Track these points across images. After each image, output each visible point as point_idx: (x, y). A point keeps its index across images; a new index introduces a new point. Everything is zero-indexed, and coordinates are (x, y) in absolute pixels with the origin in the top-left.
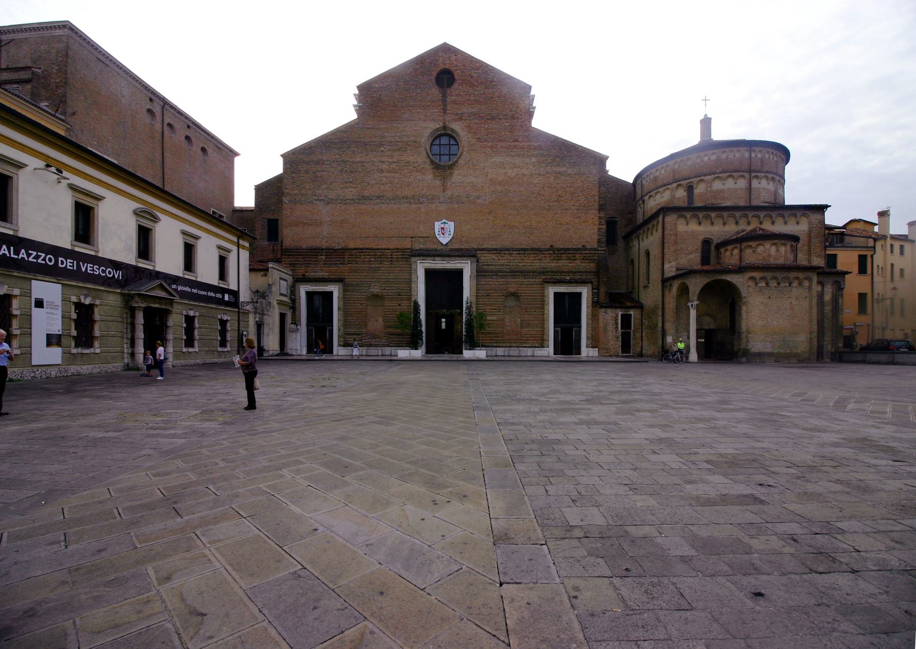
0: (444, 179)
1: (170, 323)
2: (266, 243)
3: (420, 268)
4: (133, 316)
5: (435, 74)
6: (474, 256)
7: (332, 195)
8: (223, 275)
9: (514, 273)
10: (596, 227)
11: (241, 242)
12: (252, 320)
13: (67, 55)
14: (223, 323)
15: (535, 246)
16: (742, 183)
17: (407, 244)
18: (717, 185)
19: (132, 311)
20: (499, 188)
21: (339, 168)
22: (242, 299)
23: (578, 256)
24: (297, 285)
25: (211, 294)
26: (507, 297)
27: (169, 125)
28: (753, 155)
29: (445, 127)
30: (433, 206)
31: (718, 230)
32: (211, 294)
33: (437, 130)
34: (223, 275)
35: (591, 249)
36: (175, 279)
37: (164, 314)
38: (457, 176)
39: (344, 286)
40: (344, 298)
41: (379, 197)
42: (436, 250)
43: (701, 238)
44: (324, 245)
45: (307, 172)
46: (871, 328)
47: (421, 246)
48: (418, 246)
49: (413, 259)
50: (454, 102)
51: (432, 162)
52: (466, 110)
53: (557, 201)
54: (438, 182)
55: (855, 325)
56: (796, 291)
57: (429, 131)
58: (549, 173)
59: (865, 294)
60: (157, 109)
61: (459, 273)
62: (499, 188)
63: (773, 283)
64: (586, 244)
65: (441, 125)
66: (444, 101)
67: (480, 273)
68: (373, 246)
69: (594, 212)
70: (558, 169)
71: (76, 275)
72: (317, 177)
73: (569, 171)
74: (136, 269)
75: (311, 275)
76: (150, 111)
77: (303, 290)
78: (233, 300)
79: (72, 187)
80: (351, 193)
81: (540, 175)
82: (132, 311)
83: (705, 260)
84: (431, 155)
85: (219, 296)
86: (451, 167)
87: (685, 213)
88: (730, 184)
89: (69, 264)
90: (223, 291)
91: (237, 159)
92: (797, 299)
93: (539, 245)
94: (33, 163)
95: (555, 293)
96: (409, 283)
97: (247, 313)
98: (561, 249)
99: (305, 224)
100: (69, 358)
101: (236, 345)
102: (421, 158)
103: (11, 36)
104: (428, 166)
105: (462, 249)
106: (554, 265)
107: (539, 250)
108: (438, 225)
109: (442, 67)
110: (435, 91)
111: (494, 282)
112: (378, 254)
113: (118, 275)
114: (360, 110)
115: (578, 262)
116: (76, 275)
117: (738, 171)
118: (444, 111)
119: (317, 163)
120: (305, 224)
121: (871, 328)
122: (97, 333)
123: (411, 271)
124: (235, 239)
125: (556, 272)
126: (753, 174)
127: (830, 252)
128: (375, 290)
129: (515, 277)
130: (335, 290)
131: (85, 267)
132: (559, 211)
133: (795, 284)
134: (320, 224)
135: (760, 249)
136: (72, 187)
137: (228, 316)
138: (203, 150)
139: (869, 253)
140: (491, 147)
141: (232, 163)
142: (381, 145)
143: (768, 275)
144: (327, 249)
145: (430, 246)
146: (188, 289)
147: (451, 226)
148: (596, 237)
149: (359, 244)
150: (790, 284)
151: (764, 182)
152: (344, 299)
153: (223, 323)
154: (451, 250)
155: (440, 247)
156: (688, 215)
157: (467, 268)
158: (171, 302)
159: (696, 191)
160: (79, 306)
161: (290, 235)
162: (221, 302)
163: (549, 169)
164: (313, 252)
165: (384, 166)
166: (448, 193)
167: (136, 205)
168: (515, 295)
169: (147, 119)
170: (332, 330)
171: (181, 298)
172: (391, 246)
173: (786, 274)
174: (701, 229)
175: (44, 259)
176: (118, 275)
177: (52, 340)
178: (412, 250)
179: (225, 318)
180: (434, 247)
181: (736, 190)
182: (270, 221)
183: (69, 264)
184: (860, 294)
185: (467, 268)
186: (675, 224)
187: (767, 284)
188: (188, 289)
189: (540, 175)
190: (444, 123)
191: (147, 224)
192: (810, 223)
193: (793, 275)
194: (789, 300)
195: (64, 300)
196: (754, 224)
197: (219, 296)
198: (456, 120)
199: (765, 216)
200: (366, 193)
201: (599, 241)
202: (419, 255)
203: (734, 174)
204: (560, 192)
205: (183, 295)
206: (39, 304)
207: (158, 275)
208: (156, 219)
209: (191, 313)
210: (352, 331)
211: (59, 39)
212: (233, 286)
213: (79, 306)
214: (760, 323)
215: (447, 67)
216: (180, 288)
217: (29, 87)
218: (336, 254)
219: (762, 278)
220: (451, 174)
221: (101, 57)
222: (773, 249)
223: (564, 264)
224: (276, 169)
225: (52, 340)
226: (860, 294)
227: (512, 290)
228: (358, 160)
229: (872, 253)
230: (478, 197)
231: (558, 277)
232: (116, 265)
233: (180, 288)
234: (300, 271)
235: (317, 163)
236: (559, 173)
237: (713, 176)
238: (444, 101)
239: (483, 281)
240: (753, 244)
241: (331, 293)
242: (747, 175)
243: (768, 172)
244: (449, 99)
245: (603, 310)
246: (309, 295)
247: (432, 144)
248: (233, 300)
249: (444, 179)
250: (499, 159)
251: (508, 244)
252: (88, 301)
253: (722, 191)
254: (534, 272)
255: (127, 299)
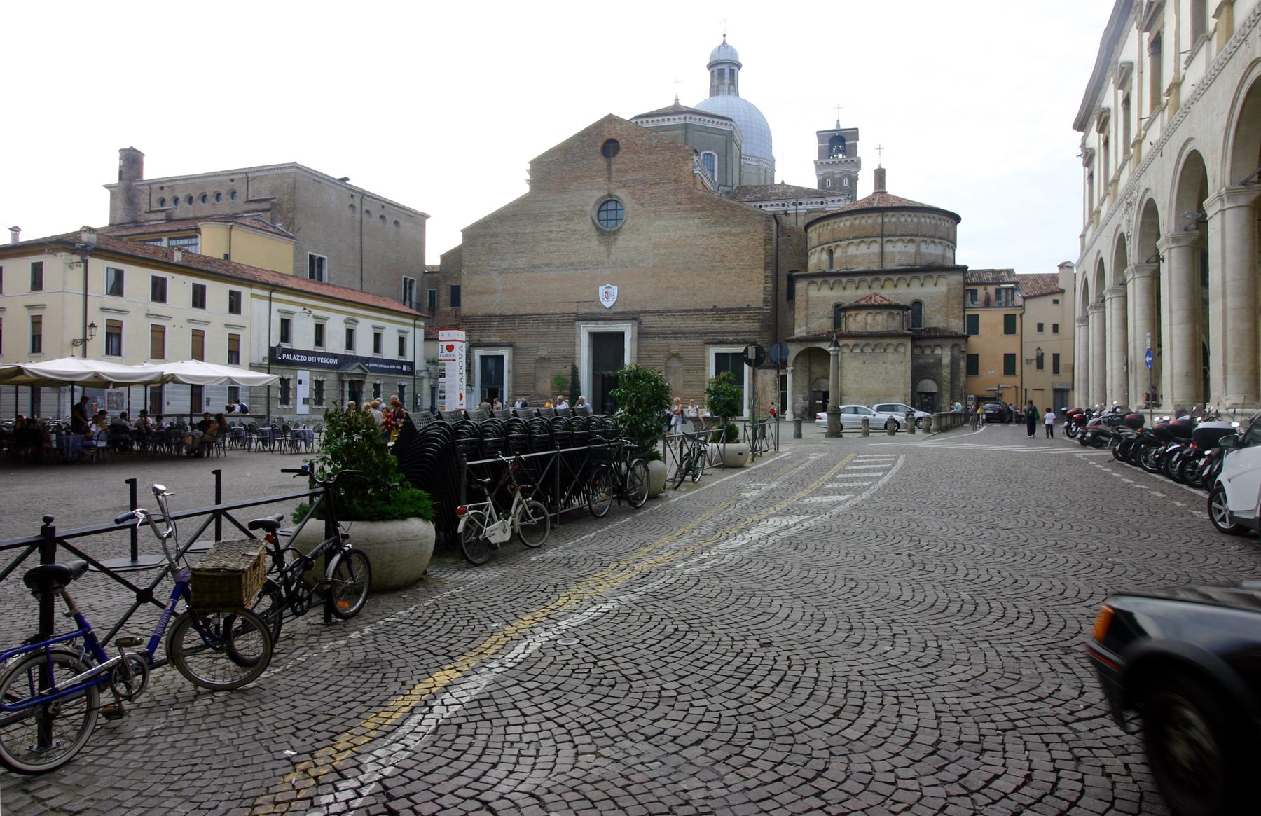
0: (609, 244)
1: (364, 390)
2: (450, 308)
3: (584, 332)
4: (343, 386)
5: (600, 144)
6: (635, 319)
7: (504, 265)
8: (401, 352)
9: (676, 334)
10: (762, 286)
11: (417, 323)
12: (426, 385)
13: (294, 188)
14: (401, 388)
15: (698, 307)
16: (875, 248)
17: (573, 309)
18: (852, 250)
19: (343, 382)
20: (662, 251)
21: (512, 239)
22: (417, 367)
23: (741, 316)
24: (472, 349)
25: (393, 367)
26: (669, 358)
27: (368, 212)
28: (886, 220)
29: (610, 195)
30: (598, 272)
31: (849, 294)
32: (393, 367)
33: (603, 198)
34: (401, 352)
35: (756, 309)
36: (368, 360)
37: (361, 383)
38: (621, 241)
39: (514, 350)
40: (513, 361)
41: (547, 265)
42: (600, 314)
43: (833, 302)
44: (498, 312)
45: (483, 245)
46: (1019, 390)
47: (586, 311)
48: (583, 310)
49: (577, 323)
50: (619, 170)
51: (598, 229)
52: (629, 177)
53: (721, 261)
54: (603, 248)
55: (999, 388)
56: (891, 356)
57: (595, 199)
58: (713, 233)
59: (1013, 355)
60: (357, 202)
61: (621, 335)
62: (662, 251)
63: (868, 350)
64: (751, 303)
65: (606, 193)
66: (609, 170)
67: (641, 335)
68: (542, 311)
69: (759, 270)
70: (722, 229)
71: (317, 365)
72: (491, 249)
73: (734, 231)
74: (345, 356)
75: (485, 340)
76: (351, 206)
77: (478, 353)
78: (409, 369)
79: (315, 317)
80: (521, 262)
81: (703, 236)
82: (343, 382)
83: (837, 322)
84: (597, 222)
85: (399, 367)
86: (615, 233)
87: (815, 280)
88: (863, 249)
89: (312, 359)
90: (402, 363)
91: (428, 222)
92: (892, 363)
93: (703, 306)
94: (299, 309)
95: (716, 354)
96: (573, 346)
97: (422, 379)
98: (724, 310)
99: (481, 293)
100: (312, 411)
101: (412, 404)
102: (586, 226)
103: (256, 174)
104: (593, 233)
105: (625, 312)
106: (717, 326)
107: (701, 311)
108: (602, 290)
109: (608, 137)
110: (601, 161)
111: (656, 344)
112: (546, 319)
113: (335, 361)
114: (531, 183)
115: (742, 322)
116: (317, 365)
117: (870, 237)
118: (609, 179)
119: (492, 236)
120: (481, 293)
121: (1019, 390)
122: (325, 397)
123: (575, 335)
124: (412, 322)
125: (718, 333)
126: (885, 239)
127: (969, 312)
128: (543, 353)
129: (676, 338)
130: (506, 353)
131: (321, 360)
132: (723, 271)
133: (890, 350)
134: (495, 292)
135: (859, 318)
136: (315, 317)
137: (406, 382)
138: (396, 223)
139: (1017, 313)
140: (654, 212)
141: (424, 226)
142: (550, 215)
143: (862, 342)
144: (500, 315)
145: (595, 310)
146: (376, 365)
147: (614, 290)
148: (761, 296)
149: (529, 310)
150: (885, 350)
151: (932, 246)
152: (514, 362)
153: (401, 388)
154: (615, 313)
155: (604, 311)
156: (819, 281)
157: (628, 330)
158: (365, 376)
159: (835, 256)
160: (316, 381)
161: (469, 304)
162: (401, 372)
163: (712, 229)
164: (489, 318)
165: (553, 236)
166: (613, 258)
167: (345, 317)
168: (677, 356)
169: (348, 212)
170: (502, 392)
171: (371, 371)
172: (558, 311)
173: (879, 341)
174: (833, 293)
175: (303, 358)
176: (335, 361)
177: (305, 401)
178: (577, 314)
179: (403, 384)
180: (598, 310)
181: (869, 255)
182: (452, 287)
183: (312, 359)
184: (1054, 355)
185: (628, 330)
186: (807, 290)
187: (862, 350)
188: (376, 365)
189: (703, 236)
190: (609, 191)
191: (351, 327)
192: (948, 284)
193: (886, 341)
194: (884, 365)
195: (311, 379)
196: (863, 292)
197: (399, 367)
198: (620, 188)
199: (886, 280)
200: (536, 262)
201: (765, 300)
202: (583, 320)
203: (866, 240)
204: (724, 252)
205: (372, 370)
206: (300, 382)
207: (357, 359)
208: (356, 322)
209: (378, 382)
210: (521, 392)
211: (288, 175)
212: (409, 358)
213: (316, 381)
214: (855, 386)
215: (612, 137)
216: (371, 365)
217: (269, 214)
218: (508, 320)
219: (855, 345)
220: (615, 239)
221: (316, 179)
222: (870, 318)
223: (727, 324)
224: (457, 241)
225: (305, 401)
226: (1054, 355)
227: (674, 351)
228: (528, 231)
229: (1021, 312)
230: (642, 261)
231: (721, 338)
232: (334, 356)
233: (371, 365)
234: (476, 336)
235: (492, 236)
236: (724, 233)
237: (847, 242)
238: (609, 170)
239: (645, 343)
240: (853, 313)
241: (502, 357)
242: (879, 240)
243: (902, 235)
244: (614, 167)
245: (762, 371)
246: (484, 358)
247: (600, 210)
248: (409, 369)
249: (609, 244)
250: (662, 223)
251: (670, 306)
252: (320, 379)
253: (856, 256)
254: (696, 333)
255: (340, 375)
